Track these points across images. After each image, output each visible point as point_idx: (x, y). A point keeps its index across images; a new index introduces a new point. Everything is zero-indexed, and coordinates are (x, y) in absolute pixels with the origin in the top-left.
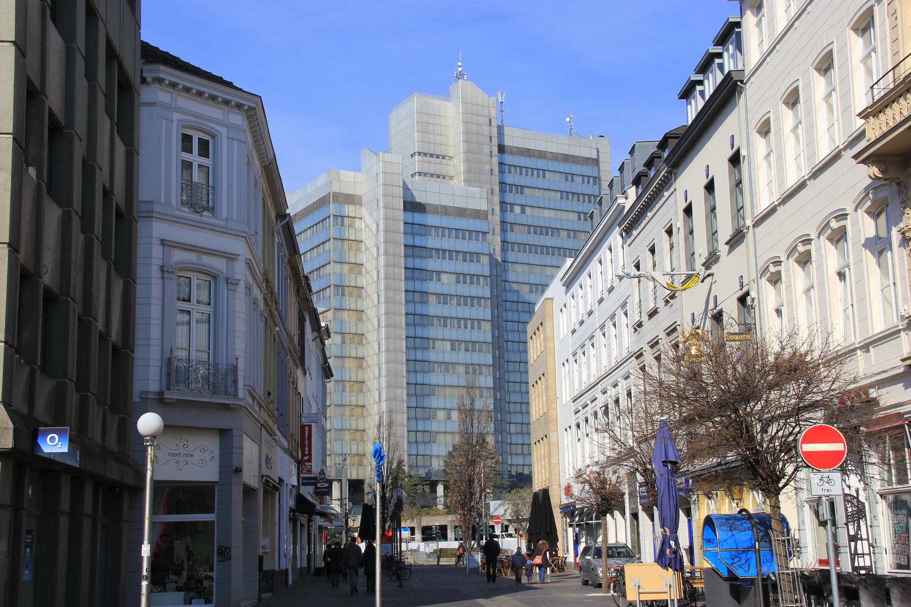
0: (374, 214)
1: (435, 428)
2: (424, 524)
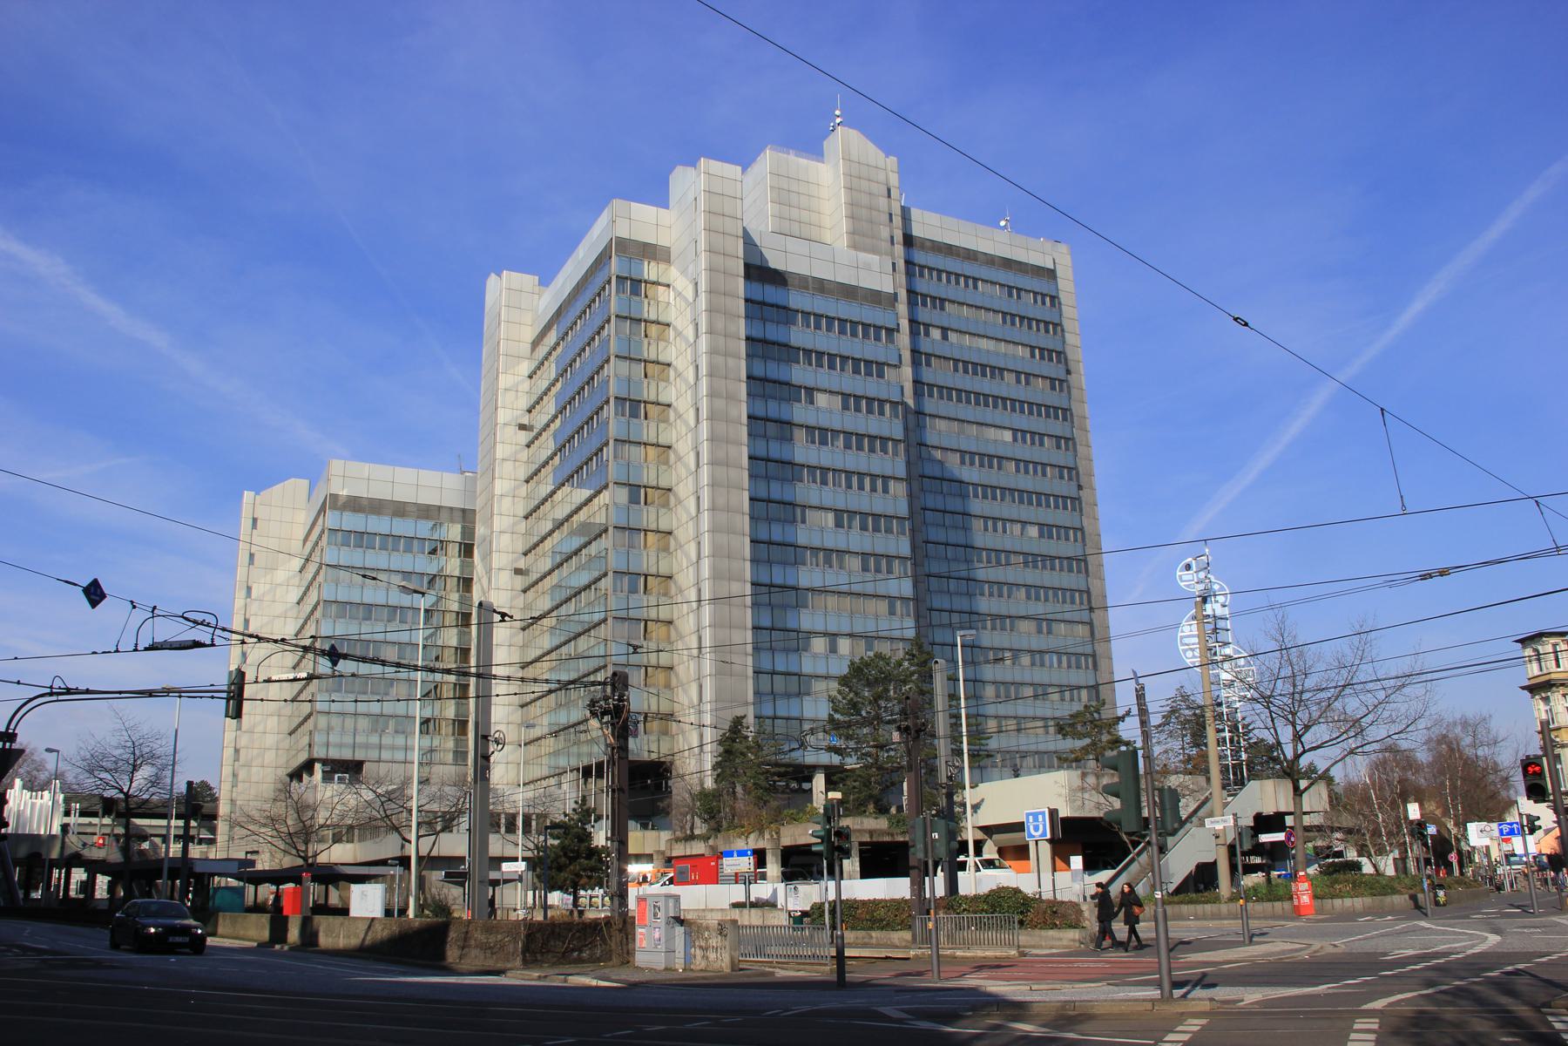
0: (691, 268)
1: (807, 666)
2: (787, 841)
